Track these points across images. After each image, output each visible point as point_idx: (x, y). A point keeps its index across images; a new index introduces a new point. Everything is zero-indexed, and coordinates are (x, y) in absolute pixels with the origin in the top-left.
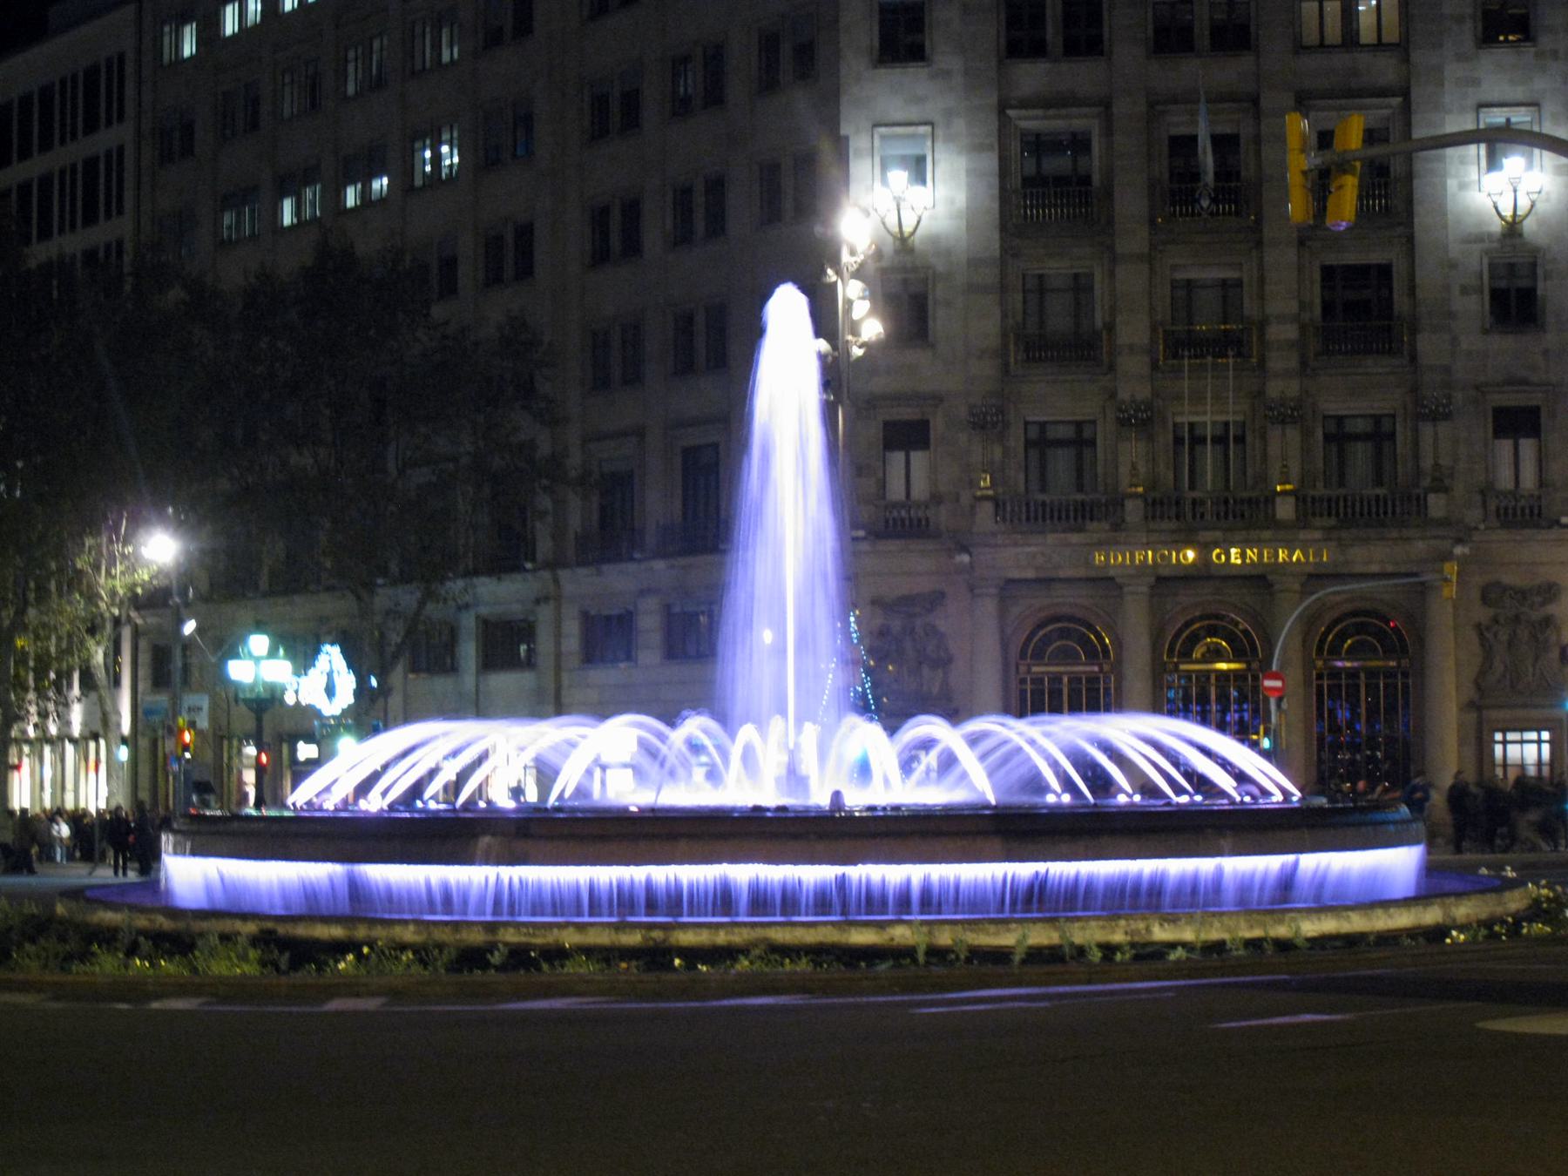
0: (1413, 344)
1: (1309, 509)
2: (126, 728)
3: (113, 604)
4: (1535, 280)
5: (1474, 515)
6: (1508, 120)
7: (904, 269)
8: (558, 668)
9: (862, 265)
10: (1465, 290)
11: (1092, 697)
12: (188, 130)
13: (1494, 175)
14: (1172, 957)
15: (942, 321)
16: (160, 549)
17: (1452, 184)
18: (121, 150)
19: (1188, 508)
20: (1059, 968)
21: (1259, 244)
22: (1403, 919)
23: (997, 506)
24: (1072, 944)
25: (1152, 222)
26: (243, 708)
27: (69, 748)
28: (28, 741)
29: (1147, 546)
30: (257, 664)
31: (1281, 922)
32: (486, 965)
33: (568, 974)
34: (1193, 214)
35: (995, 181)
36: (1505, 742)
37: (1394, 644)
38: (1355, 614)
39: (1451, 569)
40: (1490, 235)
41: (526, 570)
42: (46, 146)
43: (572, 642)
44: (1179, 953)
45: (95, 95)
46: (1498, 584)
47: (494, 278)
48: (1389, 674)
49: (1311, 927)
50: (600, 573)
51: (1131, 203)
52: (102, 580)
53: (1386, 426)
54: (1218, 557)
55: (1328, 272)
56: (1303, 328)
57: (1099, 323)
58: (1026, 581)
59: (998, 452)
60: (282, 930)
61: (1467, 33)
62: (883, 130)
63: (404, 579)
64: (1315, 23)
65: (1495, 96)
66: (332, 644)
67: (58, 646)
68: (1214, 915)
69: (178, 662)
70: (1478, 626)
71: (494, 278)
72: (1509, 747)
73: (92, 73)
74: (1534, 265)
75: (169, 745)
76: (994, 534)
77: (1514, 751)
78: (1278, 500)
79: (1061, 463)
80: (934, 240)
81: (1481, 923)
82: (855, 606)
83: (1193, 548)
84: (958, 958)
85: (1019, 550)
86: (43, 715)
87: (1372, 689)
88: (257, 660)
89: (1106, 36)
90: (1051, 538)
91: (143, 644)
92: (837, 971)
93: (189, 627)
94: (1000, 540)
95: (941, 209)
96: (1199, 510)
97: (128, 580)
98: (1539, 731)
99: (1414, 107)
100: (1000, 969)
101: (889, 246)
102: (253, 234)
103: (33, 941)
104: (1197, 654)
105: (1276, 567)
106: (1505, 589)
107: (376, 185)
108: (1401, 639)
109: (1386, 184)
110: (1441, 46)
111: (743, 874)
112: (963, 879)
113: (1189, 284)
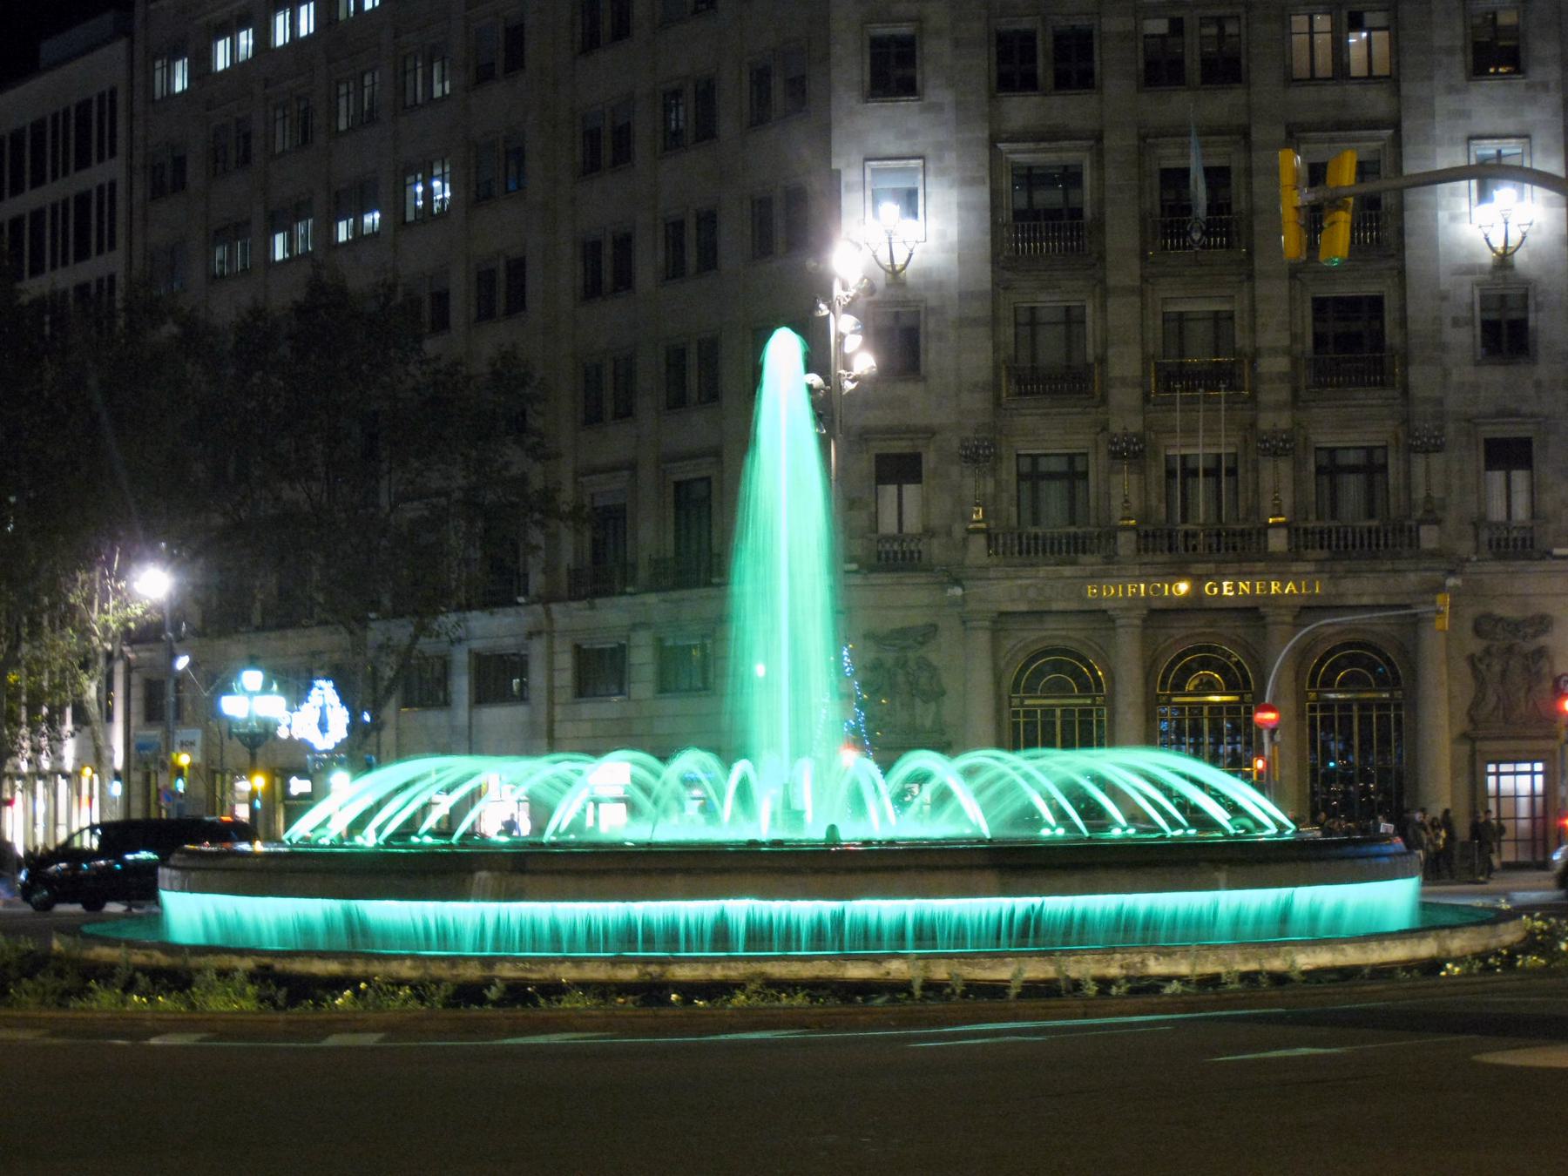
0: (1405, 376)
2: (119, 763)
3: (105, 639)
5: (1465, 547)
6: (1499, 152)
7: (897, 303)
8: (551, 703)
9: (854, 299)
10: (1456, 322)
11: (1084, 732)
12: (180, 163)
14: (1168, 990)
15: (934, 355)
16: (152, 584)
17: (1443, 216)
18: (113, 185)
20: (1053, 1002)
21: (1251, 277)
22: (1397, 952)
25: (1143, 256)
29: (1139, 579)
30: (250, 699)
31: (1277, 955)
32: (482, 1001)
33: (565, 1009)
34: (1185, 248)
36: (1498, 774)
37: (1390, 680)
38: (1046, 653)
39: (1444, 601)
40: (1481, 266)
42: (38, 181)
43: (565, 678)
44: (1175, 986)
45: (85, 130)
47: (486, 313)
48: (1383, 705)
49: (1306, 960)
50: (592, 607)
51: (1122, 237)
52: (95, 616)
53: (1378, 457)
55: (1320, 305)
56: (1294, 363)
57: (1090, 359)
58: (1022, 614)
59: (990, 486)
60: (279, 965)
61: (1457, 65)
63: (397, 614)
64: (1306, 57)
65: (1487, 128)
66: (327, 679)
68: (1210, 947)
70: (1471, 659)
71: (486, 313)
72: (1528, 777)
74: (1525, 297)
76: (987, 568)
77: (1507, 782)
78: (1271, 532)
79: (1053, 494)
80: (925, 274)
81: (1476, 956)
84: (954, 992)
85: (1008, 583)
86: (37, 750)
87: (1365, 721)
88: (251, 694)
89: (1097, 70)
92: (834, 1006)
93: (182, 663)
94: (992, 574)
95: (932, 242)
97: (121, 614)
98: (1532, 762)
101: (881, 279)
102: (244, 270)
103: (30, 977)
104: (1190, 687)
107: (368, 219)
108: (1245, 677)
110: (1431, 78)
111: (740, 909)
113: (1181, 316)
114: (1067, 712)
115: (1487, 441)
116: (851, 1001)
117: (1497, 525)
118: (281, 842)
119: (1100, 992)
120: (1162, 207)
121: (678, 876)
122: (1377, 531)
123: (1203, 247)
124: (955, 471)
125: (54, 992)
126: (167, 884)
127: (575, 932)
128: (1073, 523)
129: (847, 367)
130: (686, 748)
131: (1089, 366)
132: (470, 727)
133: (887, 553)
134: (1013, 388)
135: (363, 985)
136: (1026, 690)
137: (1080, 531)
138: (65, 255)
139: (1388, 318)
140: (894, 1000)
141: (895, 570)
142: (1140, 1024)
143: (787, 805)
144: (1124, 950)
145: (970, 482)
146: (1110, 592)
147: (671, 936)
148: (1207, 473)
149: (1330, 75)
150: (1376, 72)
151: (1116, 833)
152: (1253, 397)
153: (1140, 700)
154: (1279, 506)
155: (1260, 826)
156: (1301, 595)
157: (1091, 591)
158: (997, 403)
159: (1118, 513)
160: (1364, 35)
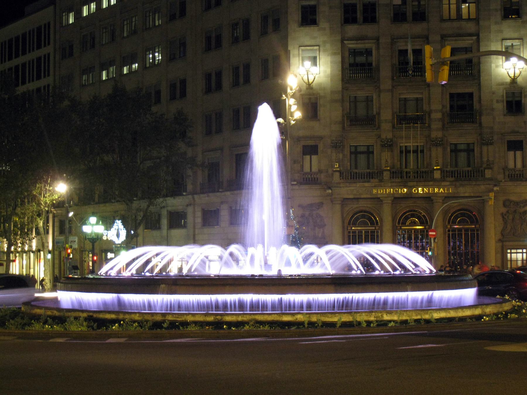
0: (480, 119)
1: (445, 174)
2: (50, 248)
3: (45, 207)
4: (521, 97)
5: (500, 177)
6: (512, 44)
7: (310, 95)
8: (194, 227)
9: (294, 94)
10: (498, 101)
11: (374, 238)
12: (71, 47)
13: (508, 63)
14: (390, 325)
15: (321, 112)
16: (61, 188)
17: (493, 65)
18: (49, 55)
19: (405, 174)
20: (352, 329)
22: (468, 313)
23: (340, 173)
24: (357, 321)
25: (393, 79)
26: (87, 242)
27: (32, 255)
28: (18, 252)
29: (391, 187)
30: (93, 227)
31: (427, 314)
32: (161, 327)
33: (189, 330)
34: (406, 76)
35: (340, 65)
36: (511, 253)
37: (473, 220)
38: (361, 211)
39: (492, 195)
40: (506, 83)
41: (183, 195)
42: (24, 53)
43: (199, 220)
44: (392, 324)
45: (40, 36)
46: (508, 200)
47: (173, 97)
48: (473, 230)
49: (436, 315)
50: (208, 196)
51: (385, 73)
52: (42, 199)
53: (471, 147)
54: (415, 191)
55: (452, 96)
56: (443, 115)
57: (375, 113)
59: (341, 156)
60: (95, 316)
61: (499, 15)
62: (303, 48)
63: (143, 198)
64: (447, 12)
66: (119, 220)
67: (27, 220)
68: (404, 311)
69: (67, 226)
70: (502, 214)
71: (173, 97)
72: (521, 254)
73: (39, 29)
74: (521, 93)
75: (63, 254)
76: (339, 183)
77: (514, 256)
78: (435, 172)
79: (362, 159)
80: (320, 84)
81: (494, 314)
82: (292, 207)
83: (406, 188)
84: (318, 325)
85: (348, 188)
86: (23, 244)
87: (466, 235)
88: (93, 225)
89: (377, 16)
90: (358, 185)
91: (56, 219)
92: (278, 330)
93: (71, 214)
94: (342, 185)
95: (322, 74)
96: (408, 175)
97: (51, 198)
98: (522, 249)
99: (480, 40)
100: (332, 329)
101: (305, 86)
102: (92, 83)
103: (13, 319)
104: (407, 223)
105: (434, 194)
106: (511, 201)
107: (134, 66)
108: (476, 219)
109: (471, 66)
111: (248, 298)
112: (377, 297)
113: (405, 100)
114: (367, 232)
115: (508, 141)
116: (284, 328)
117: (511, 170)
118: (97, 274)
119: (367, 325)
120: (399, 62)
121: (228, 287)
122: (471, 171)
123: (413, 76)
124: (329, 151)
125: (21, 324)
126: (59, 288)
127: (408, 298)
128: (368, 168)
129: (292, 116)
130: (213, 244)
131: (375, 116)
132: (167, 236)
133: (306, 178)
134: (349, 123)
135: (122, 322)
136: (402, 224)
137: (371, 171)
138: (33, 77)
139: (475, 99)
140: (298, 328)
141: (309, 184)
142: (378, 336)
143: (266, 263)
144: (376, 312)
145: (334, 154)
146: (381, 192)
147: (225, 305)
148: (414, 152)
149: (455, 18)
150: (471, 17)
151: (377, 272)
152: (429, 126)
153: (391, 228)
154: (438, 163)
155: (425, 271)
156: (445, 193)
157: (375, 191)
158: (343, 128)
159: (383, 166)
160: (467, 5)
